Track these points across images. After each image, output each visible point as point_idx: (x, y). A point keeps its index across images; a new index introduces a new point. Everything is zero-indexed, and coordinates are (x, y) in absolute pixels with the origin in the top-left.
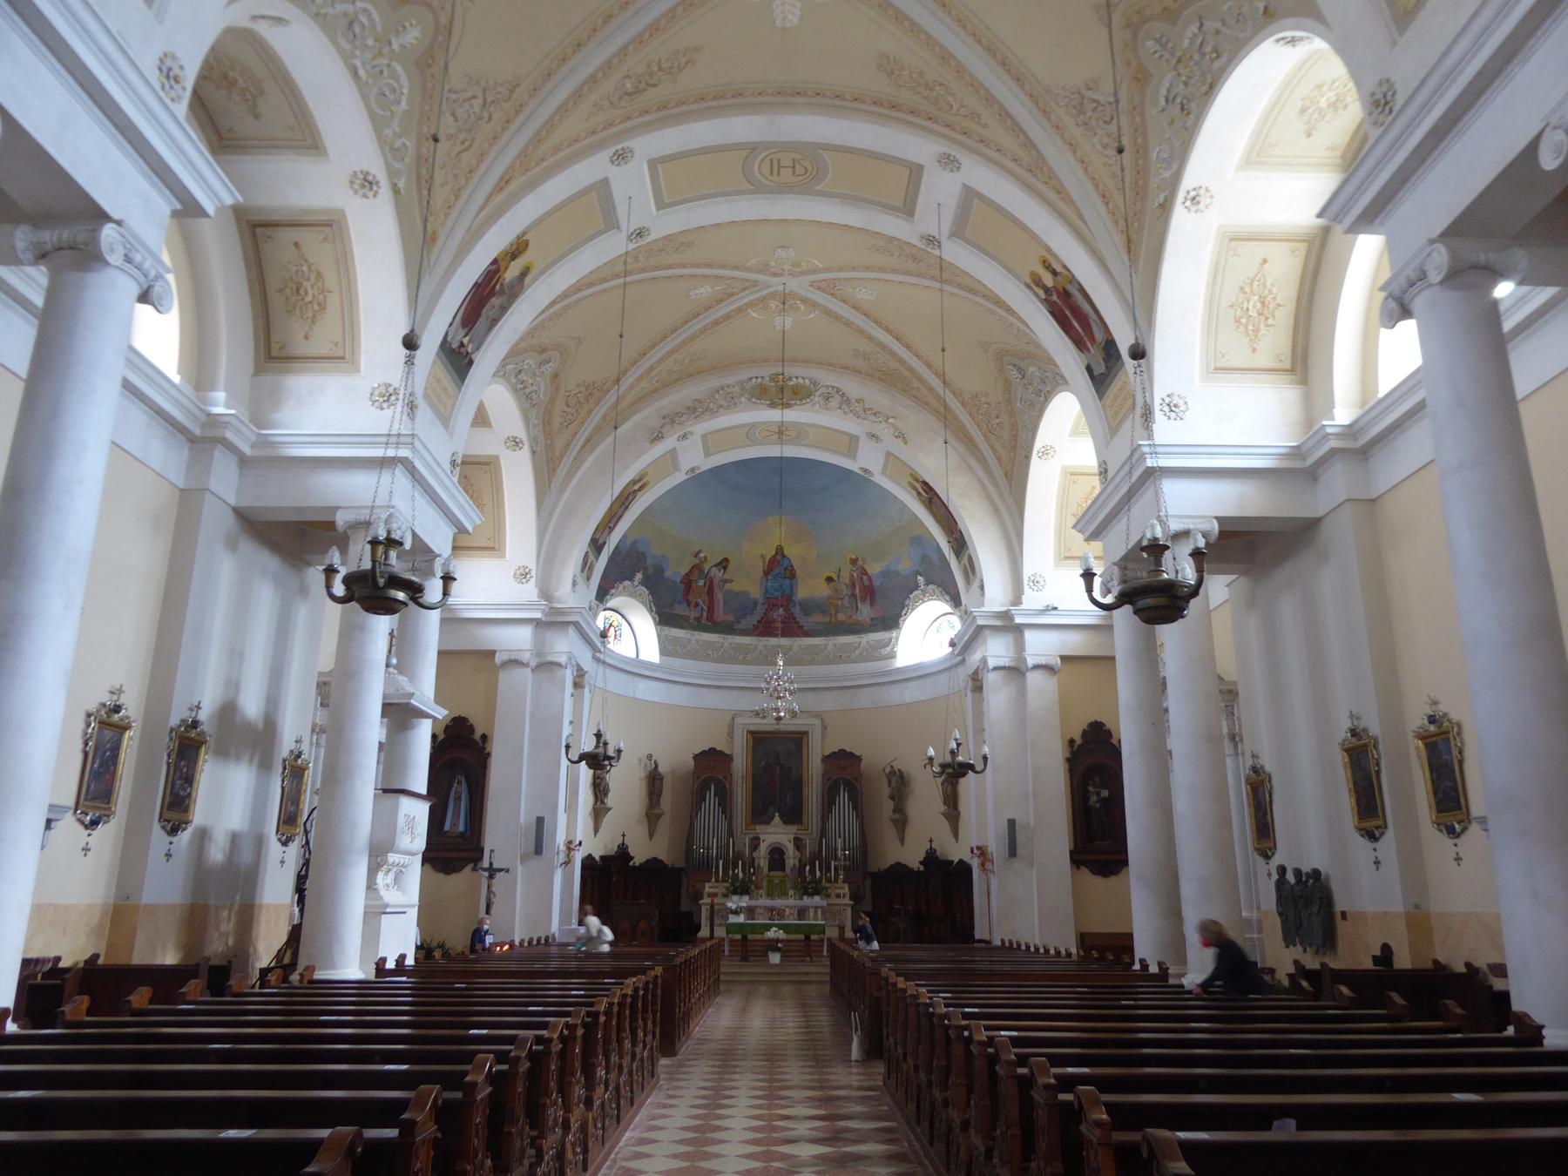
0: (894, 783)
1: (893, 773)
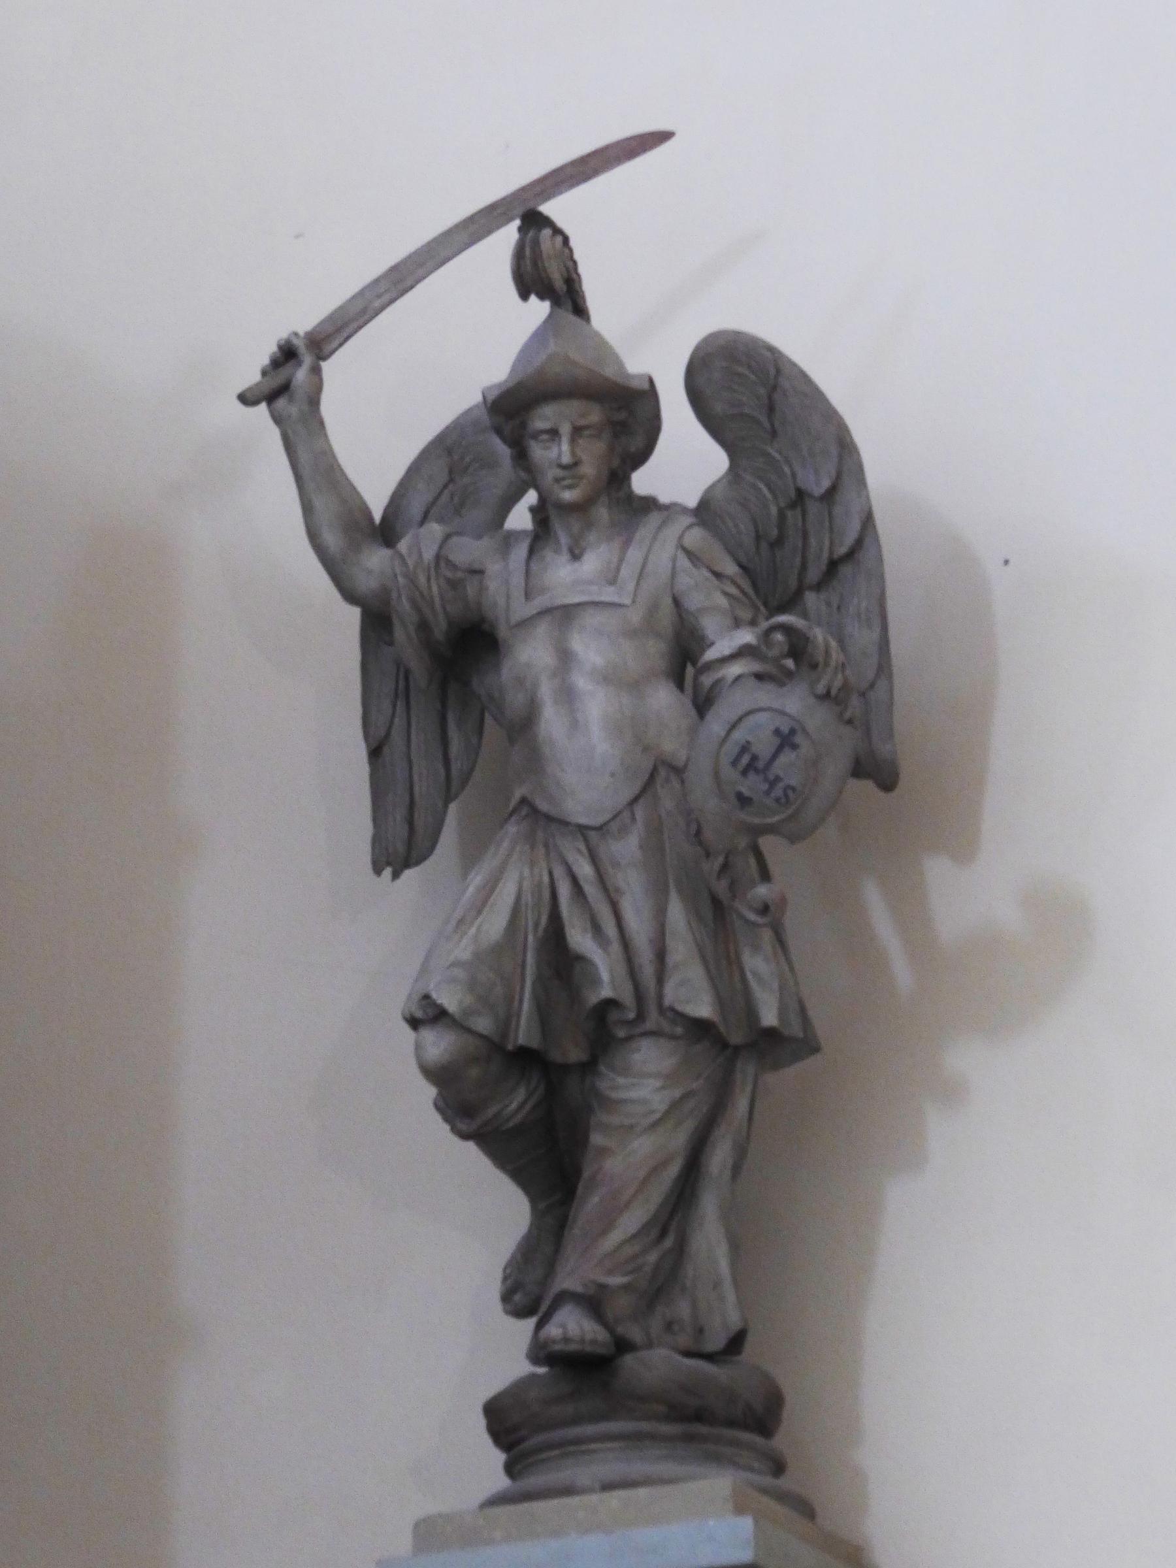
0: (587, 703)
1: (561, 425)
